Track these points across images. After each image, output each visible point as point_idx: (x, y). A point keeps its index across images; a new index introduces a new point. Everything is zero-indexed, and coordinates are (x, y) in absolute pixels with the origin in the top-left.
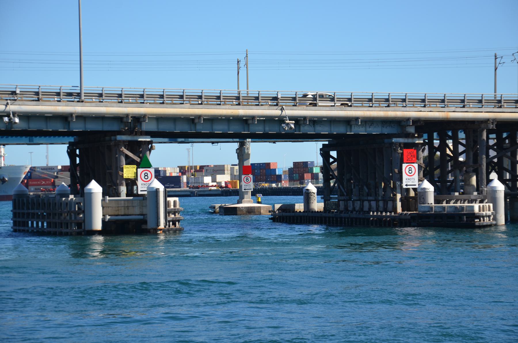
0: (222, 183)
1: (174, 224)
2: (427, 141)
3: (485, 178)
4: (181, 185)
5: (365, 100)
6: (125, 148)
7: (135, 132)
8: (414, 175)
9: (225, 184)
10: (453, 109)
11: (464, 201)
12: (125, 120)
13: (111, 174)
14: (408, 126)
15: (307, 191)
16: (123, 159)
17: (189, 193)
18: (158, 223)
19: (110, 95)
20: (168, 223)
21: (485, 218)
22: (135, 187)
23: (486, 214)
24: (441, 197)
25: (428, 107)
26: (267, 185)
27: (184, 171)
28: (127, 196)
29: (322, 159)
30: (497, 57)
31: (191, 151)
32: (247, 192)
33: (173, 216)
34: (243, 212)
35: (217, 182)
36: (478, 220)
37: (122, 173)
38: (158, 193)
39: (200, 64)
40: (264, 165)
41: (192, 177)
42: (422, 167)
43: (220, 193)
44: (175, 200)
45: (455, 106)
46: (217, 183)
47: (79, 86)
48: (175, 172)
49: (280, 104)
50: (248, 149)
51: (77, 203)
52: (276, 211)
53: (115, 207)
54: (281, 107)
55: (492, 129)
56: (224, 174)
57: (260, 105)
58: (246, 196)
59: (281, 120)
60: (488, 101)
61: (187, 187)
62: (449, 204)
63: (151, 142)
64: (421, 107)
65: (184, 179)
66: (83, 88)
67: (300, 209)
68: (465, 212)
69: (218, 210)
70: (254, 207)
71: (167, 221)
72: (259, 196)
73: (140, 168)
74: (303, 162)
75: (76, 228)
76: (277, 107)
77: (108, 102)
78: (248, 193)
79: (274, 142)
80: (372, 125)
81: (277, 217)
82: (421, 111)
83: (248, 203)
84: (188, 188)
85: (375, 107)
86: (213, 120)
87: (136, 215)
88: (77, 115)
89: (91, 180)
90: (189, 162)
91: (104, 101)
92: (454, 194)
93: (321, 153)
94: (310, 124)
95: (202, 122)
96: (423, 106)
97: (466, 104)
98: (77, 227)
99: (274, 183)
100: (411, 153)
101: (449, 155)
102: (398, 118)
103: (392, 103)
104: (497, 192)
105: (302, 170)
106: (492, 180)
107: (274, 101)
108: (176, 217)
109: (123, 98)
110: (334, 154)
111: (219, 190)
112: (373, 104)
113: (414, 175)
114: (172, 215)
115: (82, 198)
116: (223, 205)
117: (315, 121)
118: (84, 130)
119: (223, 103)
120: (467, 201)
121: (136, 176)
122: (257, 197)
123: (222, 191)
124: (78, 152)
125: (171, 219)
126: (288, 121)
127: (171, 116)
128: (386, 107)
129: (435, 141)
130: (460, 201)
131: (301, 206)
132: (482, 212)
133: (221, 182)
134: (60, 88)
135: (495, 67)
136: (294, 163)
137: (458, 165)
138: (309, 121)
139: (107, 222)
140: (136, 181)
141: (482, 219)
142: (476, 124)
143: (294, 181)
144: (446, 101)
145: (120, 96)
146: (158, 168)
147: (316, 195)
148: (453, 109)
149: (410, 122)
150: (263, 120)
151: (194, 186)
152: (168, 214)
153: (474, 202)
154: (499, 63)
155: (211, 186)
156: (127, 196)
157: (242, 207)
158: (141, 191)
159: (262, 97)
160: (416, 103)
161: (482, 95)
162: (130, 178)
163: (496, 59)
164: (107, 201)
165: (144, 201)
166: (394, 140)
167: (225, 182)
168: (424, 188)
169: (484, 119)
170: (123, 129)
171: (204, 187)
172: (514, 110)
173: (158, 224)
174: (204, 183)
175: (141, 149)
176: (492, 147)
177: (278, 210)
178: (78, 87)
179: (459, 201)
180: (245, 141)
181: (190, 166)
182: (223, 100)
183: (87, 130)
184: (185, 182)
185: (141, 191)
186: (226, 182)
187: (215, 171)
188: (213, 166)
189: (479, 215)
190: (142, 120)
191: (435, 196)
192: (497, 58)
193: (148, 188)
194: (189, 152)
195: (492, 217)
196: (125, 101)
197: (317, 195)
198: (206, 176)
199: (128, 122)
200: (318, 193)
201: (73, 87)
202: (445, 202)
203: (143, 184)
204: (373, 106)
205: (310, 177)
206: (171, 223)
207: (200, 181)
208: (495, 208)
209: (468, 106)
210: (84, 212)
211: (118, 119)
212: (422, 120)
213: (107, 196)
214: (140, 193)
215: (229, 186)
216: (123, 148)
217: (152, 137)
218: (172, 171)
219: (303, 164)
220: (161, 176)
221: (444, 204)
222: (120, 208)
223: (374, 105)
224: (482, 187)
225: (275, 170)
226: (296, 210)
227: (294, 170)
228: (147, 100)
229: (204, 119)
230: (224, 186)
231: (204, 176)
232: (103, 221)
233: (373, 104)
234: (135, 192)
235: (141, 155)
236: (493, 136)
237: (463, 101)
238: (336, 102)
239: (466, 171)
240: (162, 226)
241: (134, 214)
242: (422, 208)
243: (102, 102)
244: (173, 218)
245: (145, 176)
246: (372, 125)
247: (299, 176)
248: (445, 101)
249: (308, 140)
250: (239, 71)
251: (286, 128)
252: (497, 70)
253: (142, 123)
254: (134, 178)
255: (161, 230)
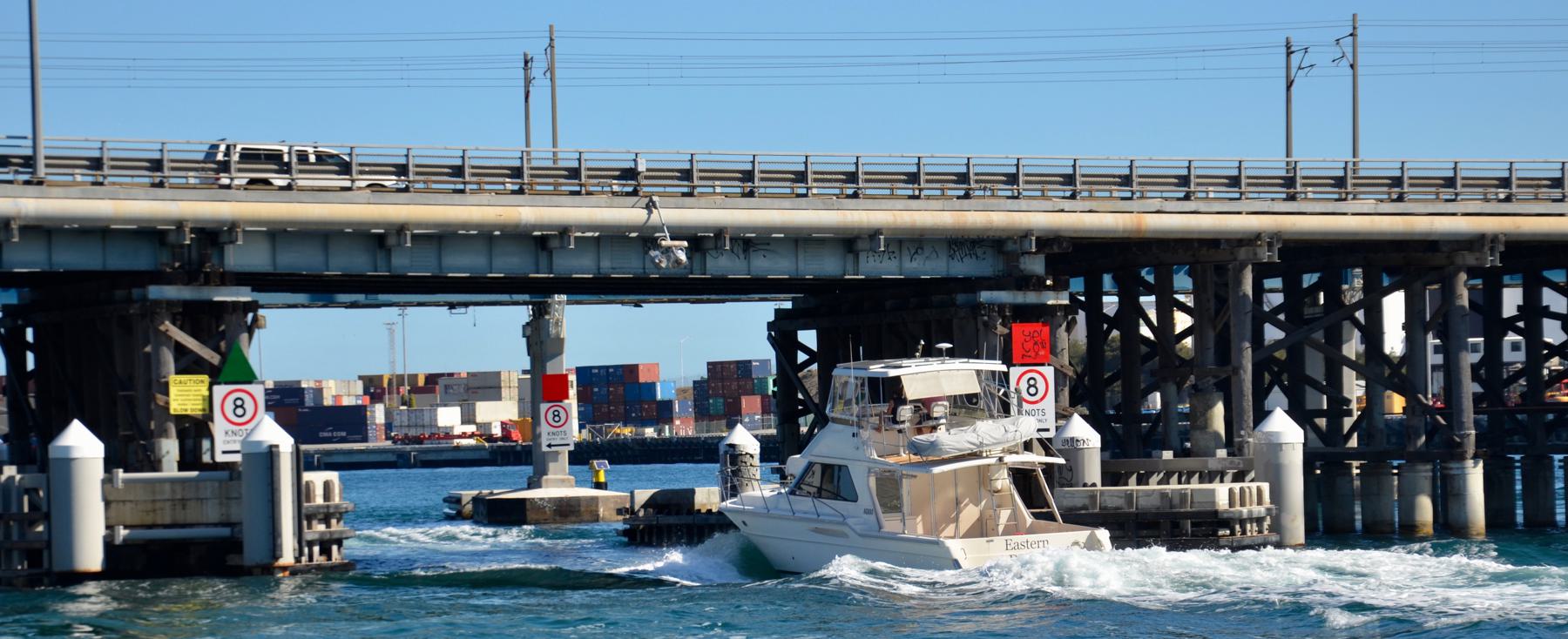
0: (493, 425)
1: (326, 551)
2: (1083, 298)
3: (1251, 409)
4: (367, 433)
5: (899, 177)
6: (174, 324)
7: (202, 276)
8: (1042, 399)
9: (503, 429)
10: (1156, 204)
11: (1190, 475)
12: (172, 238)
13: (130, 402)
14: (1027, 256)
15: (732, 449)
16: (168, 358)
17: (392, 458)
18: (275, 550)
19: (125, 165)
20: (306, 550)
21: (1248, 526)
22: (206, 444)
23: (1250, 512)
24: (1123, 464)
25: (1083, 199)
26: (627, 432)
27: (379, 391)
28: (181, 468)
29: (1477, 361)
30: (1293, 49)
31: (398, 329)
32: (557, 453)
33: (322, 527)
34: (545, 512)
35: (477, 424)
36: (1228, 532)
37: (164, 397)
38: (275, 458)
39: (410, 67)
40: (619, 372)
41: (402, 408)
42: (1065, 375)
43: (485, 455)
44: (329, 479)
45: (1165, 195)
46: (479, 426)
47: (30, 135)
48: (352, 396)
49: (645, 189)
50: (557, 323)
51: (27, 491)
52: (639, 510)
53: (145, 501)
54: (647, 200)
55: (1270, 265)
56: (499, 398)
57: (583, 192)
58: (552, 466)
59: (647, 239)
60: (1259, 182)
61: (388, 438)
62: (1147, 484)
63: (253, 306)
64: (1064, 198)
65: (378, 414)
66: (42, 143)
67: (711, 504)
68: (1189, 509)
69: (469, 507)
70: (578, 499)
71: (304, 543)
72: (599, 465)
73: (219, 383)
74: (738, 363)
75: (26, 566)
76: (635, 199)
77: (120, 184)
78: (560, 456)
79: (637, 305)
80: (919, 251)
81: (641, 527)
82: (1062, 211)
83: (559, 485)
84: (389, 443)
85: (928, 197)
86: (442, 237)
87: (207, 525)
88: (22, 223)
89: (72, 420)
90: (393, 363)
91: (106, 182)
92: (1161, 457)
93: (770, 335)
94: (735, 251)
95: (409, 245)
96: (1068, 194)
97: (1192, 189)
98: (26, 563)
99: (650, 425)
100: (1036, 334)
101: (1145, 340)
102: (997, 230)
103: (978, 186)
104: (1281, 450)
105: (734, 386)
106: (1269, 412)
107: (624, 182)
108: (332, 529)
109: (167, 173)
110: (808, 338)
111: (483, 448)
112: (920, 190)
113: (1042, 399)
114: (320, 523)
115: (43, 476)
116: (485, 492)
117: (749, 242)
118: (47, 268)
119: (475, 187)
120: (1197, 475)
121: (207, 407)
122: (592, 467)
123: (493, 451)
124: (30, 335)
125: (316, 536)
126: (667, 243)
127: (315, 227)
128: (959, 198)
129: (1106, 299)
130: (1176, 476)
131: (713, 493)
132: (1238, 508)
133: (490, 424)
134: (100, 146)
135: (1287, 77)
136: (709, 364)
137: (1182, 367)
138: (731, 239)
139: (118, 546)
140: (210, 424)
141: (1238, 527)
142: (1222, 247)
143: (711, 418)
144: (1136, 180)
145: (157, 165)
146: (299, 382)
147: (756, 461)
148: (1156, 204)
149: (1031, 244)
150: (592, 237)
151: (406, 434)
152: (305, 523)
153: (1218, 479)
154: (1300, 68)
155: (459, 437)
156: (181, 468)
157: (541, 499)
158: (224, 452)
159: (589, 169)
160: (539, 180)
161: (1240, 162)
162: (189, 413)
163: (1289, 54)
164: (120, 485)
165: (233, 482)
166: (985, 296)
167: (502, 423)
168: (1072, 439)
169: (1244, 233)
170: (167, 265)
171: (439, 438)
172: (1331, 207)
173: (275, 551)
174: (439, 428)
175: (222, 328)
176: (1271, 317)
177: (645, 506)
178: (25, 138)
179: (1176, 476)
180: (549, 300)
181: (398, 376)
182: (475, 179)
183: (55, 268)
184: (381, 425)
185: (224, 452)
186: (506, 424)
187: (470, 391)
188: (465, 376)
189: (1231, 515)
190: (224, 238)
191: (1103, 463)
192: (1292, 52)
193: (244, 443)
194: (391, 332)
195: (1267, 523)
196: (172, 181)
197: (762, 460)
198: (445, 405)
199: (182, 246)
200: (765, 456)
201: (9, 137)
202: (1133, 479)
203: (230, 433)
204: (922, 196)
205: (759, 405)
206: (316, 549)
207: (427, 421)
208: (1277, 495)
209: (1204, 195)
210: (47, 518)
211: (150, 234)
212: (1065, 238)
213: (118, 467)
214: (220, 458)
215: (516, 435)
216: (167, 323)
217: (256, 289)
218: (340, 390)
219: (738, 368)
220: (307, 405)
221: (1132, 486)
222: (158, 505)
223: (924, 193)
224: (1242, 433)
225: (652, 386)
226: (697, 507)
227: (709, 386)
228: (766, 187)
229: (414, 237)
230: (500, 435)
231: (438, 405)
232: (109, 545)
233: (920, 190)
234: (206, 458)
235: (223, 344)
236: (1277, 283)
237: (1184, 181)
238: (355, 176)
239: (1194, 387)
240: (287, 557)
241: (205, 518)
242: (1064, 497)
243: (101, 184)
244: (322, 533)
245: (237, 407)
246: (919, 251)
247: (726, 404)
248: (103, 164)
249: (737, 297)
250: (531, 89)
251: (660, 261)
252: (1293, 88)
253: (226, 247)
254: (203, 415)
255: (284, 568)
